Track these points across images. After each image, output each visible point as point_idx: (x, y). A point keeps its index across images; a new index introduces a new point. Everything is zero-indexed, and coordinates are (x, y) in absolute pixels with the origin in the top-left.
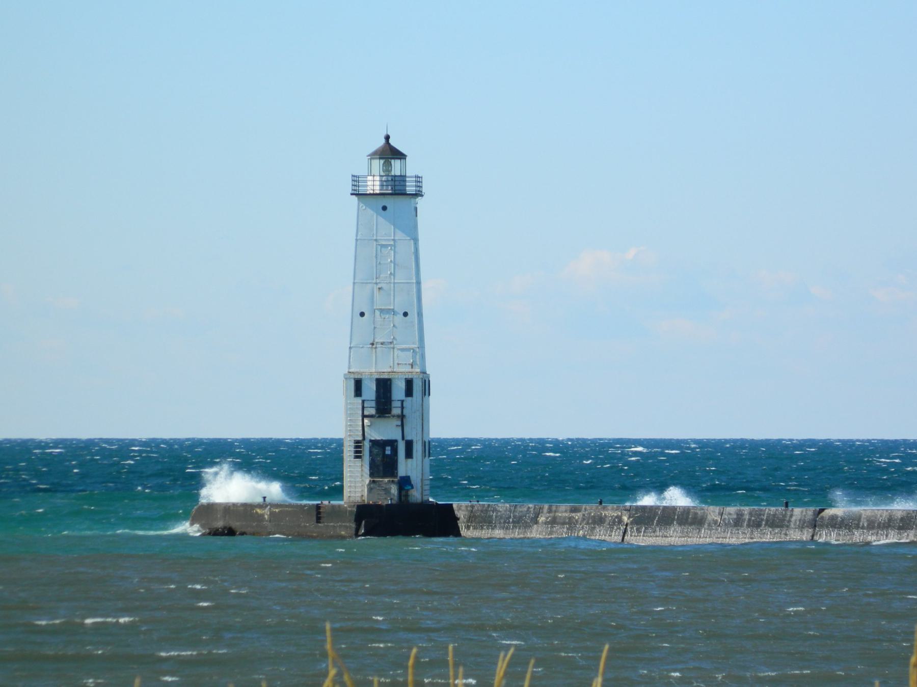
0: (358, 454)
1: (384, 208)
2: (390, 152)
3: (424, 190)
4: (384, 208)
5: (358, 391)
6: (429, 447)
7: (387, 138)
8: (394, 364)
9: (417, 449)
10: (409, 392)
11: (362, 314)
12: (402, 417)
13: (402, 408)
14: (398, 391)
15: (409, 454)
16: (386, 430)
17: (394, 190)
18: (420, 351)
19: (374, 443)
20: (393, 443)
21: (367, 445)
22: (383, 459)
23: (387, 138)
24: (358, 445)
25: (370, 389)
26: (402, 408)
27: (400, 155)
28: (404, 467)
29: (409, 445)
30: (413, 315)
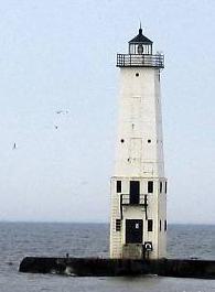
0: (118, 228)
1: (137, 75)
2: (141, 40)
3: (165, 64)
4: (137, 75)
5: (119, 190)
6: (165, 226)
7: (141, 31)
8: (143, 173)
9: (155, 226)
10: (150, 189)
11: (141, 55)
12: (146, 205)
13: (146, 199)
14: (143, 189)
15: (150, 229)
16: (135, 214)
17: (33, 266)
18: (160, 163)
19: (129, 222)
20: (141, 222)
21: (124, 221)
22: (134, 232)
23: (141, 31)
24: (118, 222)
25: (126, 189)
26: (146, 199)
27: (149, 42)
28: (146, 236)
29: (150, 223)
30: (154, 142)
